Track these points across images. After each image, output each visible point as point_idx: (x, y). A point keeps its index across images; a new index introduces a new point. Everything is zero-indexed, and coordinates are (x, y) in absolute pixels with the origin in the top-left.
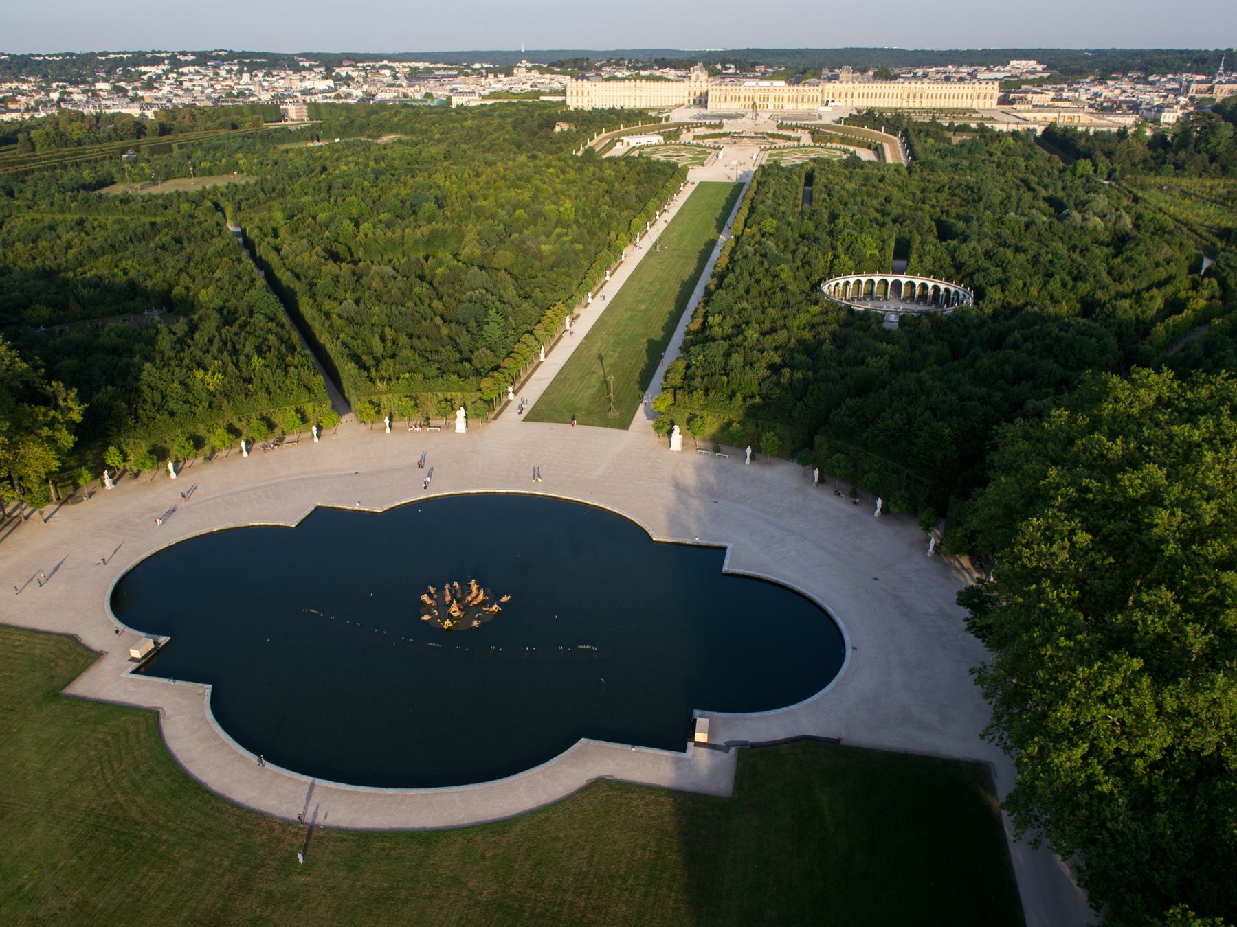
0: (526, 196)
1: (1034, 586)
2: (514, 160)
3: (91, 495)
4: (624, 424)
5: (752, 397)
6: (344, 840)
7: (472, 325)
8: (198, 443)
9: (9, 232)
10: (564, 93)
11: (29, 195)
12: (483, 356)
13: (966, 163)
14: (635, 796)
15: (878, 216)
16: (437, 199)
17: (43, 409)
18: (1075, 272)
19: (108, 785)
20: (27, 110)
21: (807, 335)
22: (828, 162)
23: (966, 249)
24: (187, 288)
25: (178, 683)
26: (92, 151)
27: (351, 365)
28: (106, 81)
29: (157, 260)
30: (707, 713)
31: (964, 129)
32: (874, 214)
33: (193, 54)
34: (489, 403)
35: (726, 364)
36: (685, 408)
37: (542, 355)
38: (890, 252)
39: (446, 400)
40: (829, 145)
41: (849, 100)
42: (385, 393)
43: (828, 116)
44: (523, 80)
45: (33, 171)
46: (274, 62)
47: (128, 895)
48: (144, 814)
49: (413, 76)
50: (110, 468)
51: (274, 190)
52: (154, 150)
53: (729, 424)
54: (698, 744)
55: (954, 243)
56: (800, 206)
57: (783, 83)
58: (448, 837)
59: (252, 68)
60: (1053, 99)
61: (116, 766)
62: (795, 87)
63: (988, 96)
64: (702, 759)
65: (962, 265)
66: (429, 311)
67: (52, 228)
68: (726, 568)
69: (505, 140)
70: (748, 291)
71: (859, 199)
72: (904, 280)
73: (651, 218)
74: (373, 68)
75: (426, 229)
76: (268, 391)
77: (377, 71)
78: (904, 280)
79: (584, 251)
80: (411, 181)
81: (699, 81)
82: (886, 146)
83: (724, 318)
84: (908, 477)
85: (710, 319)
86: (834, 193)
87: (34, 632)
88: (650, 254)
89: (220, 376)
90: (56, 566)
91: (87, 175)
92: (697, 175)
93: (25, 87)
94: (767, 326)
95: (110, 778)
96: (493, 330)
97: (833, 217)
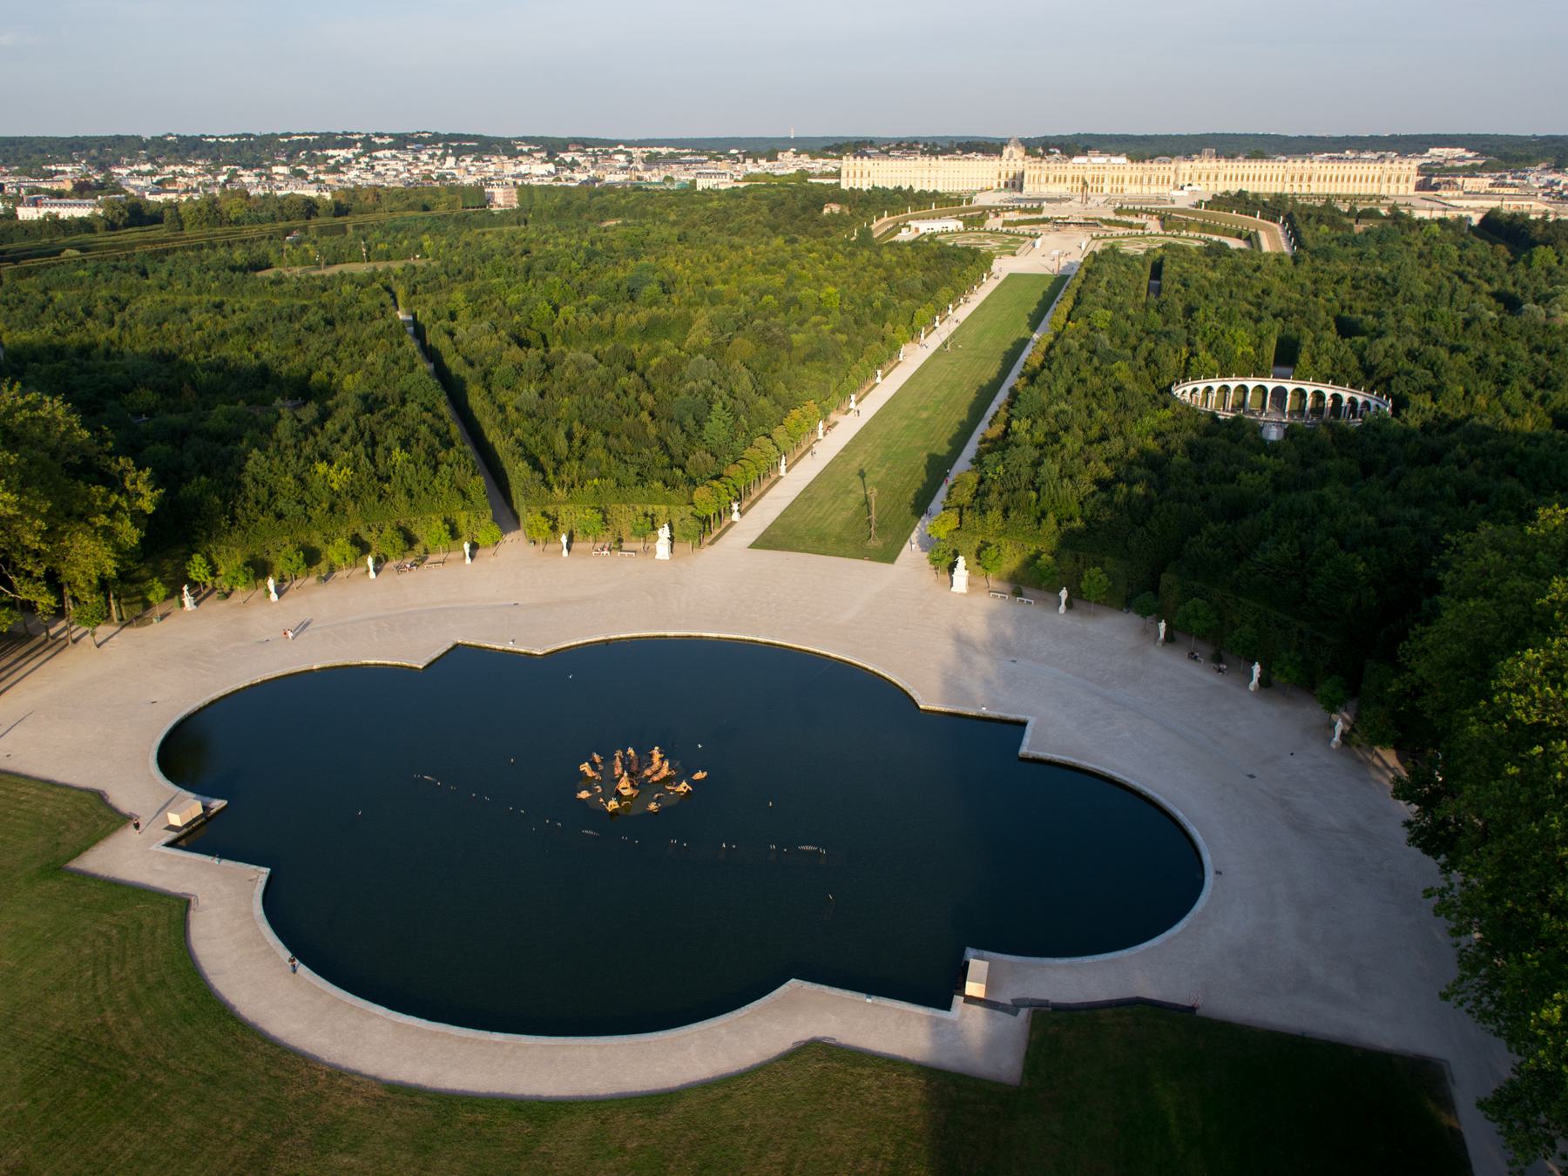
0: (778, 281)
1: (1538, 749)
2: (767, 244)
3: (163, 617)
4: (889, 556)
5: (1070, 519)
6: (416, 1105)
7: (689, 422)
8: (311, 557)
9: (132, 315)
10: (838, 175)
11: (164, 275)
12: (700, 457)
13: (1374, 251)
14: (867, 1072)
15: (1253, 310)
16: (662, 284)
17: (102, 490)
18: (1541, 379)
19: (97, 999)
20: (186, 191)
21: (1151, 444)
22: (1184, 249)
23: (1381, 346)
24: (330, 375)
25: (225, 862)
26: (251, 231)
27: (523, 465)
28: (284, 164)
29: (299, 342)
30: (986, 953)
31: (1370, 214)
32: (1246, 307)
33: (391, 136)
34: (706, 520)
35: (1037, 474)
36: (975, 533)
37: (783, 468)
38: (1270, 351)
39: (646, 515)
40: (1184, 233)
41: (1212, 184)
42: (565, 503)
43: (1183, 199)
44: (788, 164)
45: (175, 250)
46: (485, 147)
47: (89, 1162)
48: (137, 1043)
49: (652, 161)
50: (194, 585)
51: (460, 272)
52: (323, 231)
53: (1037, 556)
54: (971, 1000)
55: (1360, 340)
56: (1151, 299)
57: (1122, 160)
58: (573, 1112)
59: (459, 153)
60: (1492, 185)
61: (114, 970)
62: (1140, 165)
63: (1403, 179)
64: (972, 1024)
65: (1374, 367)
66: (635, 406)
67: (185, 311)
68: (1025, 750)
69: (758, 222)
70: (1069, 391)
71: (1226, 290)
72: (1290, 387)
73: (941, 310)
74: (606, 153)
75: (643, 315)
76: (410, 493)
77: (609, 156)
78: (1290, 387)
79: (848, 343)
80: (632, 263)
81: (1014, 160)
82: (1263, 235)
83: (1035, 422)
84: (1301, 633)
85: (1015, 424)
86: (1193, 284)
87: (51, 784)
88: (938, 353)
89: (348, 471)
90: (97, 709)
91: (239, 256)
92: (1004, 266)
93: (191, 170)
94: (1095, 432)
95: (102, 987)
96: (716, 427)
97: (1190, 311)
